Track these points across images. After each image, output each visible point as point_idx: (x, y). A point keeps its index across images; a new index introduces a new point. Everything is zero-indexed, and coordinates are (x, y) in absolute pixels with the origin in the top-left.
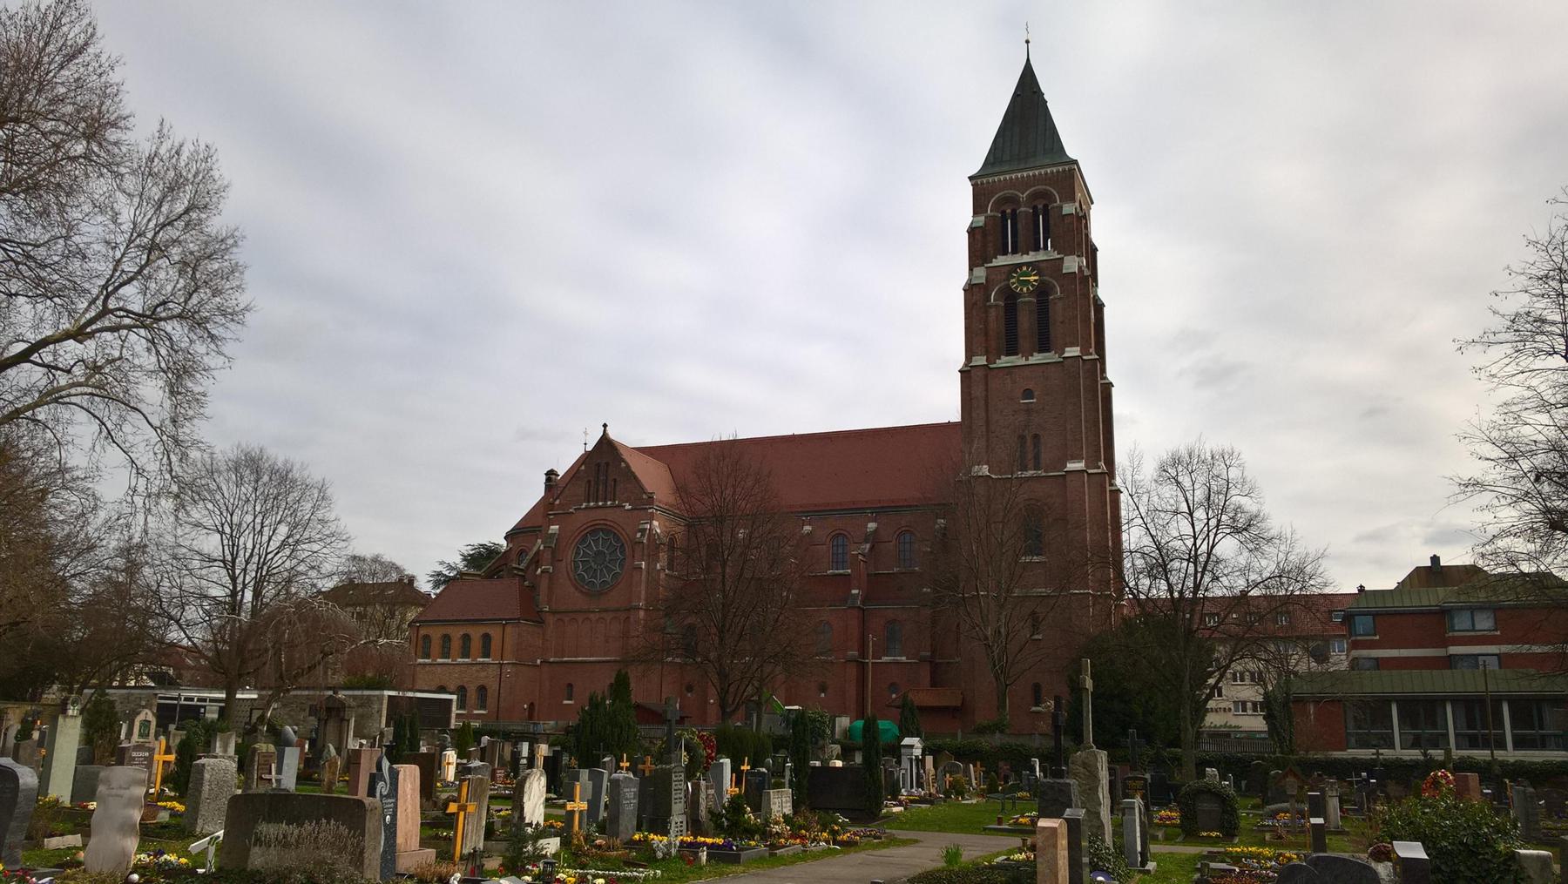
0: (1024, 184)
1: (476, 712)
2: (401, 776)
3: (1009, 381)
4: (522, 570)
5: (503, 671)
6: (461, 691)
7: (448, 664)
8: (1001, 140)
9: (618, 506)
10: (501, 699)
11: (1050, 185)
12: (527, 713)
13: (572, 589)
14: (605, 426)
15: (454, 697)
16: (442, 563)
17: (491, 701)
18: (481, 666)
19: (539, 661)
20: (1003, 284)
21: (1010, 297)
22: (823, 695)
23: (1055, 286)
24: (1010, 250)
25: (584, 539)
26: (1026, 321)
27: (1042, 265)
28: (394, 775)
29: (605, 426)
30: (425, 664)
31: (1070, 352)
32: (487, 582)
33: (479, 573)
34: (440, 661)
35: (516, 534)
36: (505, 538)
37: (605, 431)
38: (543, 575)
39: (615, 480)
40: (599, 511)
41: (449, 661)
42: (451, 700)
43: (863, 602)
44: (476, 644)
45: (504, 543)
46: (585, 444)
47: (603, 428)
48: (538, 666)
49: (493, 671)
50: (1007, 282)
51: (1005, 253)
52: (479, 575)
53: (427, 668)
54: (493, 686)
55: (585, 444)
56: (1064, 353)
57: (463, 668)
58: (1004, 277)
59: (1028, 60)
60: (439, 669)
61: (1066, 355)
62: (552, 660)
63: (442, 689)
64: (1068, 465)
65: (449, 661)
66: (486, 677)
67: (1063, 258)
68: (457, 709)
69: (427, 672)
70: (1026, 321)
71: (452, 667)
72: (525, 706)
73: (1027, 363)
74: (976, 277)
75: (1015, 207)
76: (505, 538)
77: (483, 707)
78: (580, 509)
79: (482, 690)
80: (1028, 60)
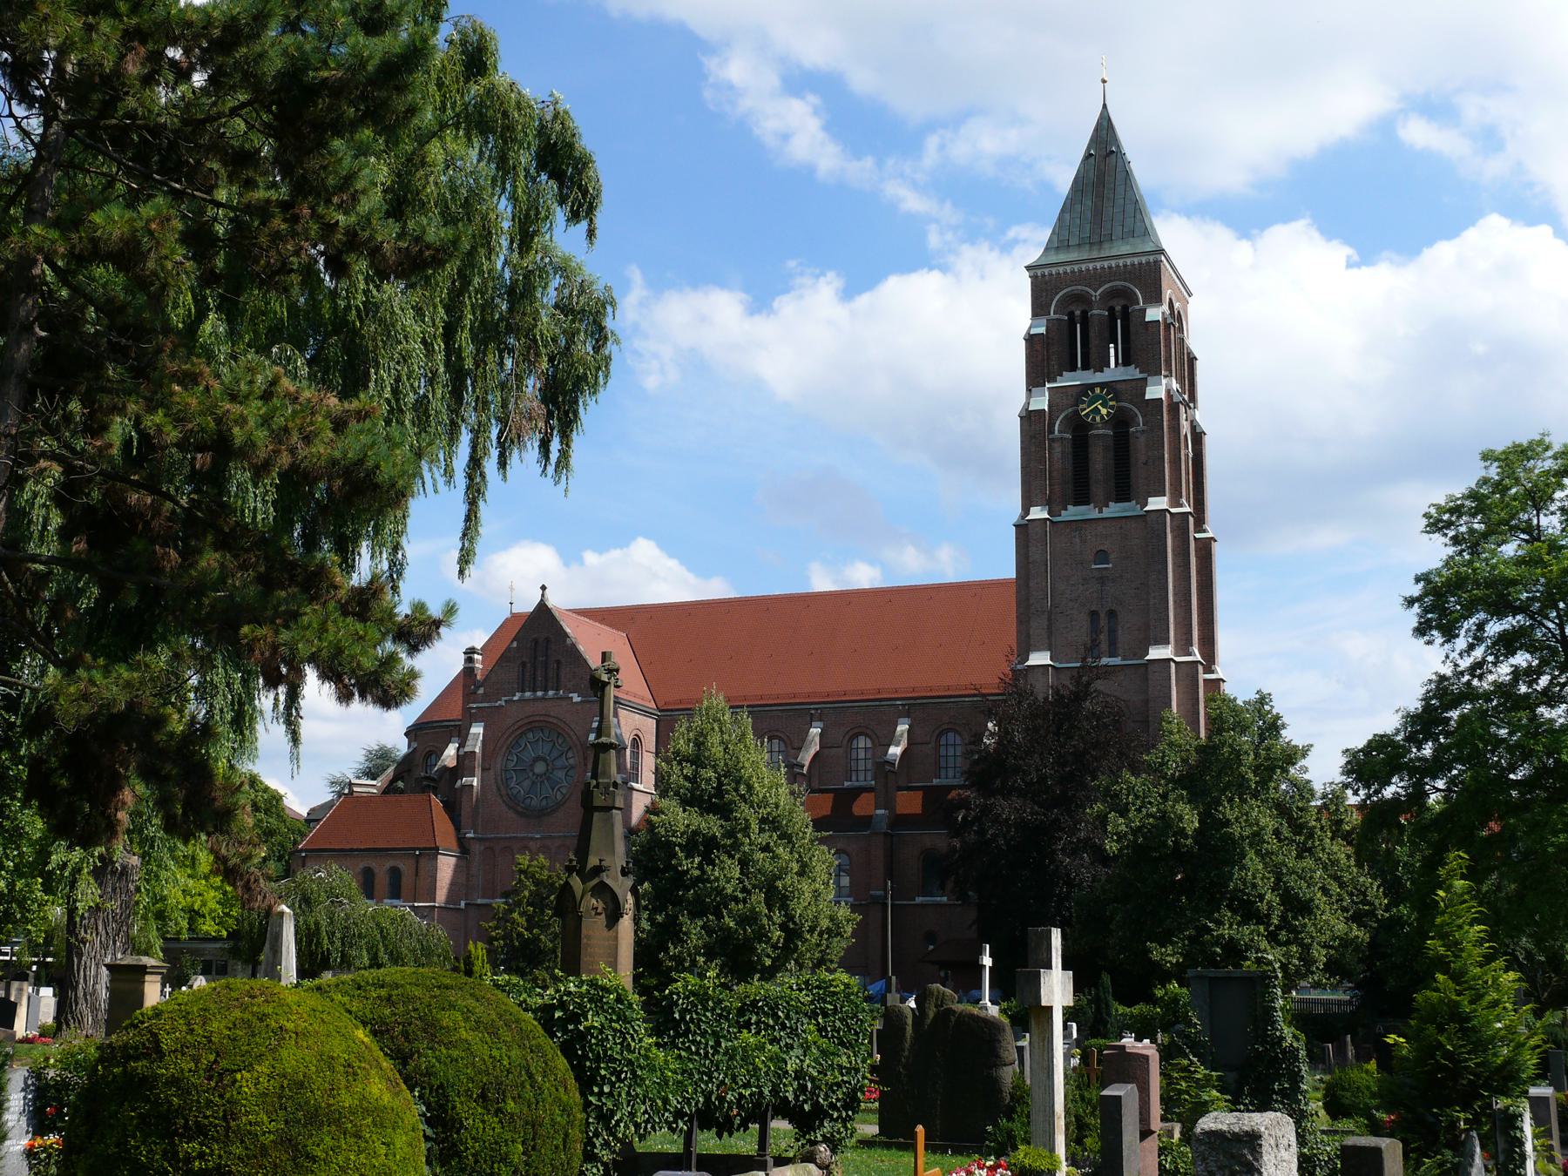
3: (1078, 540)
8: (1067, 216)
20: (1070, 410)
24: (1079, 365)
26: (1099, 460)
27: (1118, 386)
31: (1155, 503)
37: (543, 595)
51: (1073, 368)
59: (1105, 106)
70: (1099, 460)
73: (1100, 516)
80: (1105, 106)
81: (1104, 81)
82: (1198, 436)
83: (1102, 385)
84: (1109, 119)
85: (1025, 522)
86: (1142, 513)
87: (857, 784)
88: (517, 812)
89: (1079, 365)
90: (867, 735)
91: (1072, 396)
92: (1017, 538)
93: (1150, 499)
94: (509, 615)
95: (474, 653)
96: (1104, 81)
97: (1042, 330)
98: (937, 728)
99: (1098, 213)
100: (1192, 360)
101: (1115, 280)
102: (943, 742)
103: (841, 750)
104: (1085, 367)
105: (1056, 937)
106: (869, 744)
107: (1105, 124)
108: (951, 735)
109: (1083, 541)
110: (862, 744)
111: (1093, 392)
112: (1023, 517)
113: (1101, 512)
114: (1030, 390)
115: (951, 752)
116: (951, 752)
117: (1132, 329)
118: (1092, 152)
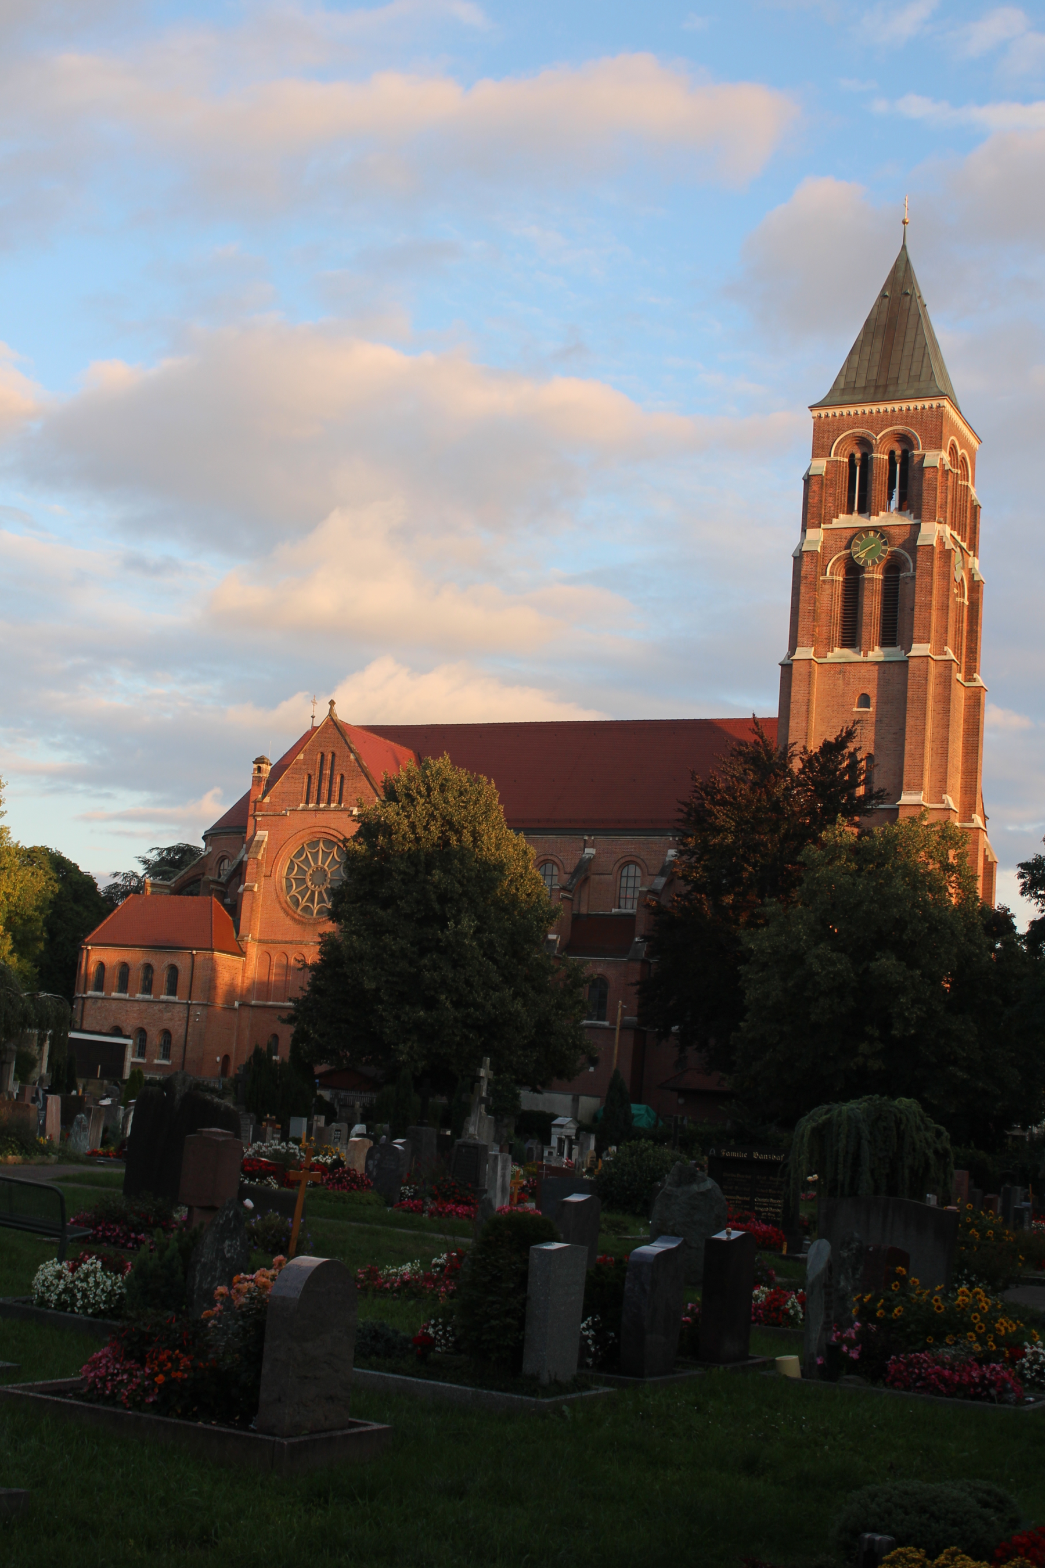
0: (882, 421)
1: (156, 1061)
2: (49, 1102)
3: (840, 682)
4: (221, 884)
5: (192, 1013)
6: (141, 1034)
7: (125, 1000)
8: (856, 358)
9: (345, 810)
10: (188, 1048)
11: (911, 426)
12: (220, 1068)
13: (282, 914)
14: (332, 703)
15: (129, 1042)
16: (116, 875)
17: (176, 1050)
18: (164, 1005)
19: (236, 1004)
20: (843, 552)
21: (853, 571)
22: (592, 1069)
23: (908, 561)
24: (856, 508)
25: (314, 844)
26: (872, 605)
27: (892, 531)
28: (45, 1100)
29: (332, 703)
30: (97, 998)
31: (918, 649)
32: (176, 898)
33: (168, 883)
34: (114, 994)
35: (215, 834)
36: (204, 838)
37: (331, 709)
38: (583, 841)
39: (342, 777)
40: (319, 815)
41: (127, 996)
42: (124, 1046)
43: (560, 951)
44: (161, 977)
45: (202, 845)
46: (313, 717)
47: (329, 706)
48: (235, 1009)
49: (180, 1012)
50: (848, 551)
51: (850, 511)
52: (168, 886)
53: (99, 1003)
54: (178, 1031)
55: (313, 717)
56: (910, 651)
57: (143, 1006)
58: (844, 543)
59: (904, 247)
60: (114, 1005)
61: (911, 654)
62: (253, 1002)
63: (117, 1032)
64: (903, 797)
65: (127, 996)
66: (171, 1019)
67: (920, 524)
68: (133, 1057)
69: (99, 1008)
70: (872, 605)
71: (129, 1004)
72: (218, 1059)
73: (865, 659)
74: (809, 542)
75: (867, 451)
76: (204, 838)
77: (166, 1056)
78: (296, 810)
79: (167, 1033)
80: (904, 247)
81: (904, 223)
82: (975, 587)
83: (875, 529)
84: (908, 261)
85: (789, 662)
86: (905, 659)
87: (624, 911)
88: (294, 919)
89: (856, 508)
90: (636, 864)
91: (846, 538)
92: (782, 678)
93: (914, 646)
94: (309, 728)
95: (263, 763)
96: (904, 223)
97: (822, 471)
98: (637, 857)
99: (887, 355)
100: (976, 509)
101: (896, 424)
102: (625, 873)
103: (611, 877)
104: (862, 510)
105: (100, 1067)
106: (639, 873)
107: (903, 266)
108: (632, 867)
109: (847, 684)
110: (632, 873)
111: (867, 535)
112: (789, 657)
113: (866, 655)
114: (805, 531)
115: (631, 884)
116: (631, 884)
117: (910, 474)
118: (887, 294)
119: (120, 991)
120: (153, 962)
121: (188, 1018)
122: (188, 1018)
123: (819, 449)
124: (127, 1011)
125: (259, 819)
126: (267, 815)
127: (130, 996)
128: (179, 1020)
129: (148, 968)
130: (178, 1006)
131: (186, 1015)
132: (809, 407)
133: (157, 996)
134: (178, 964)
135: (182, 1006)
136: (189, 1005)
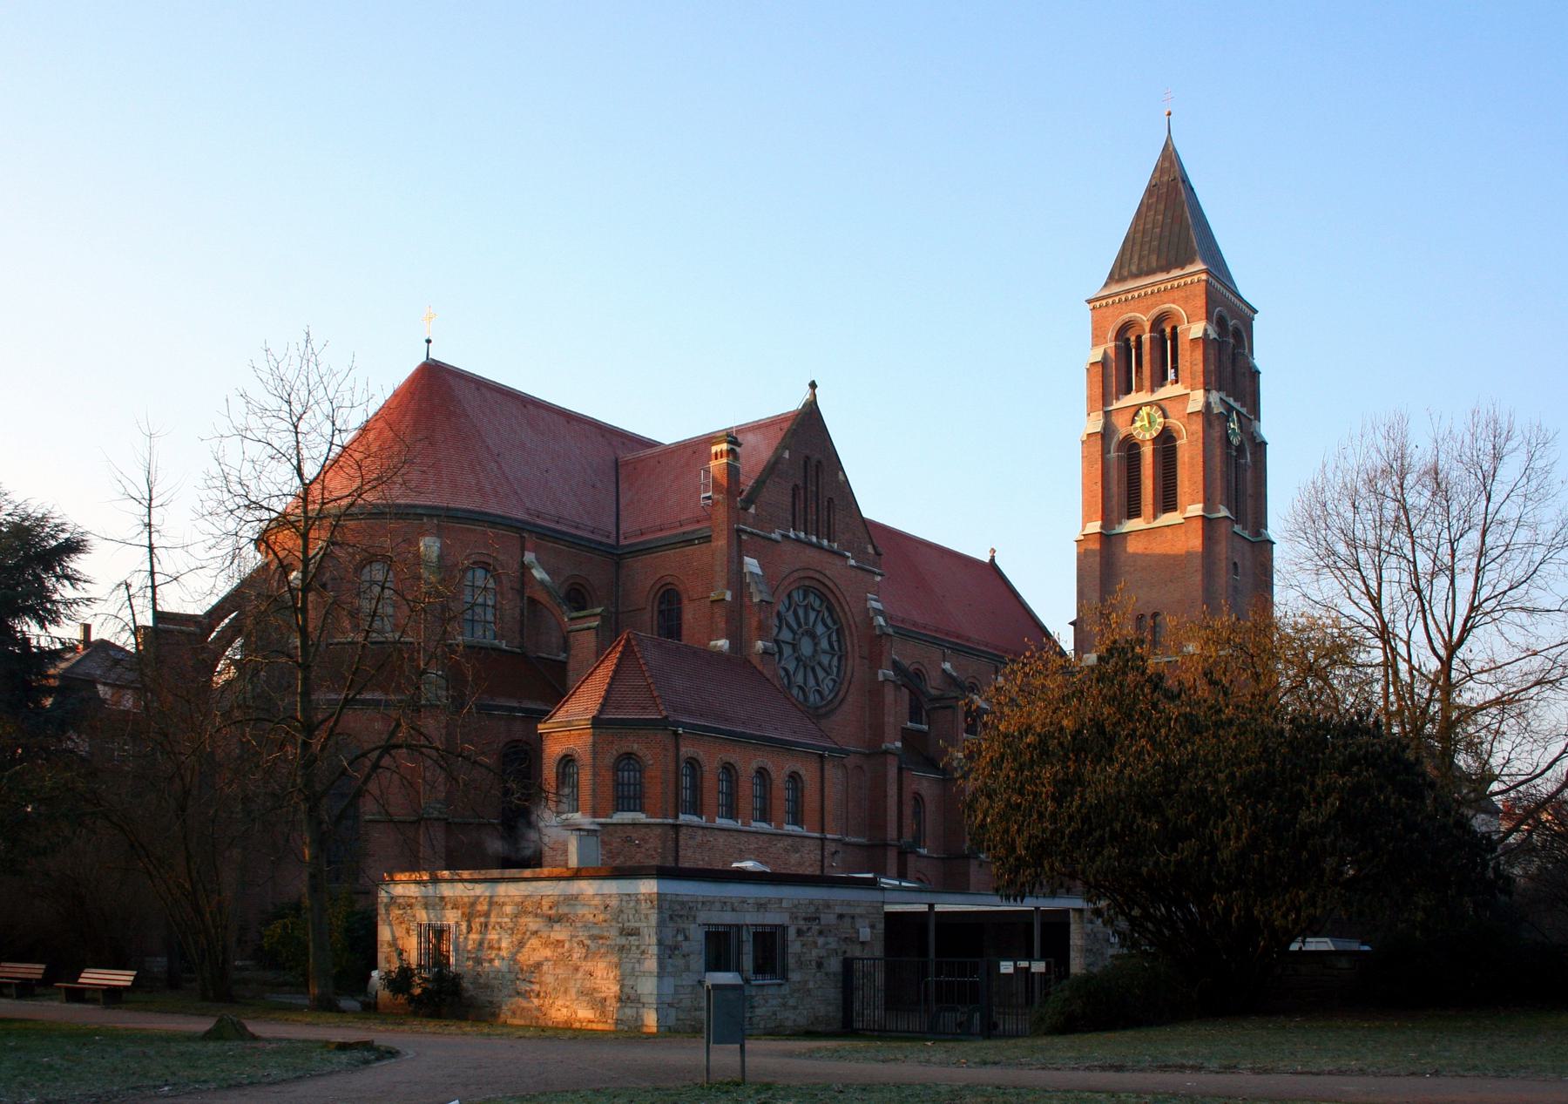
60: (721, 839)
65: (739, 825)
119: (795, 823)
120: (770, 766)
121: (822, 861)
122: (822, 861)
123: (1097, 339)
124: (741, 850)
125: (744, 537)
126: (758, 535)
127: (744, 824)
128: (811, 865)
129: (762, 773)
130: (807, 841)
131: (819, 857)
132: (1089, 302)
133: (779, 826)
134: (739, 765)
135: (812, 841)
136: (676, 827)
